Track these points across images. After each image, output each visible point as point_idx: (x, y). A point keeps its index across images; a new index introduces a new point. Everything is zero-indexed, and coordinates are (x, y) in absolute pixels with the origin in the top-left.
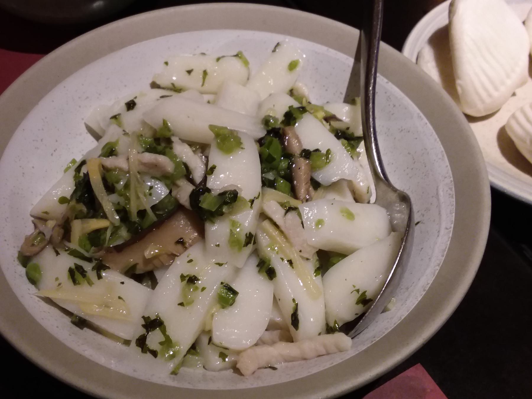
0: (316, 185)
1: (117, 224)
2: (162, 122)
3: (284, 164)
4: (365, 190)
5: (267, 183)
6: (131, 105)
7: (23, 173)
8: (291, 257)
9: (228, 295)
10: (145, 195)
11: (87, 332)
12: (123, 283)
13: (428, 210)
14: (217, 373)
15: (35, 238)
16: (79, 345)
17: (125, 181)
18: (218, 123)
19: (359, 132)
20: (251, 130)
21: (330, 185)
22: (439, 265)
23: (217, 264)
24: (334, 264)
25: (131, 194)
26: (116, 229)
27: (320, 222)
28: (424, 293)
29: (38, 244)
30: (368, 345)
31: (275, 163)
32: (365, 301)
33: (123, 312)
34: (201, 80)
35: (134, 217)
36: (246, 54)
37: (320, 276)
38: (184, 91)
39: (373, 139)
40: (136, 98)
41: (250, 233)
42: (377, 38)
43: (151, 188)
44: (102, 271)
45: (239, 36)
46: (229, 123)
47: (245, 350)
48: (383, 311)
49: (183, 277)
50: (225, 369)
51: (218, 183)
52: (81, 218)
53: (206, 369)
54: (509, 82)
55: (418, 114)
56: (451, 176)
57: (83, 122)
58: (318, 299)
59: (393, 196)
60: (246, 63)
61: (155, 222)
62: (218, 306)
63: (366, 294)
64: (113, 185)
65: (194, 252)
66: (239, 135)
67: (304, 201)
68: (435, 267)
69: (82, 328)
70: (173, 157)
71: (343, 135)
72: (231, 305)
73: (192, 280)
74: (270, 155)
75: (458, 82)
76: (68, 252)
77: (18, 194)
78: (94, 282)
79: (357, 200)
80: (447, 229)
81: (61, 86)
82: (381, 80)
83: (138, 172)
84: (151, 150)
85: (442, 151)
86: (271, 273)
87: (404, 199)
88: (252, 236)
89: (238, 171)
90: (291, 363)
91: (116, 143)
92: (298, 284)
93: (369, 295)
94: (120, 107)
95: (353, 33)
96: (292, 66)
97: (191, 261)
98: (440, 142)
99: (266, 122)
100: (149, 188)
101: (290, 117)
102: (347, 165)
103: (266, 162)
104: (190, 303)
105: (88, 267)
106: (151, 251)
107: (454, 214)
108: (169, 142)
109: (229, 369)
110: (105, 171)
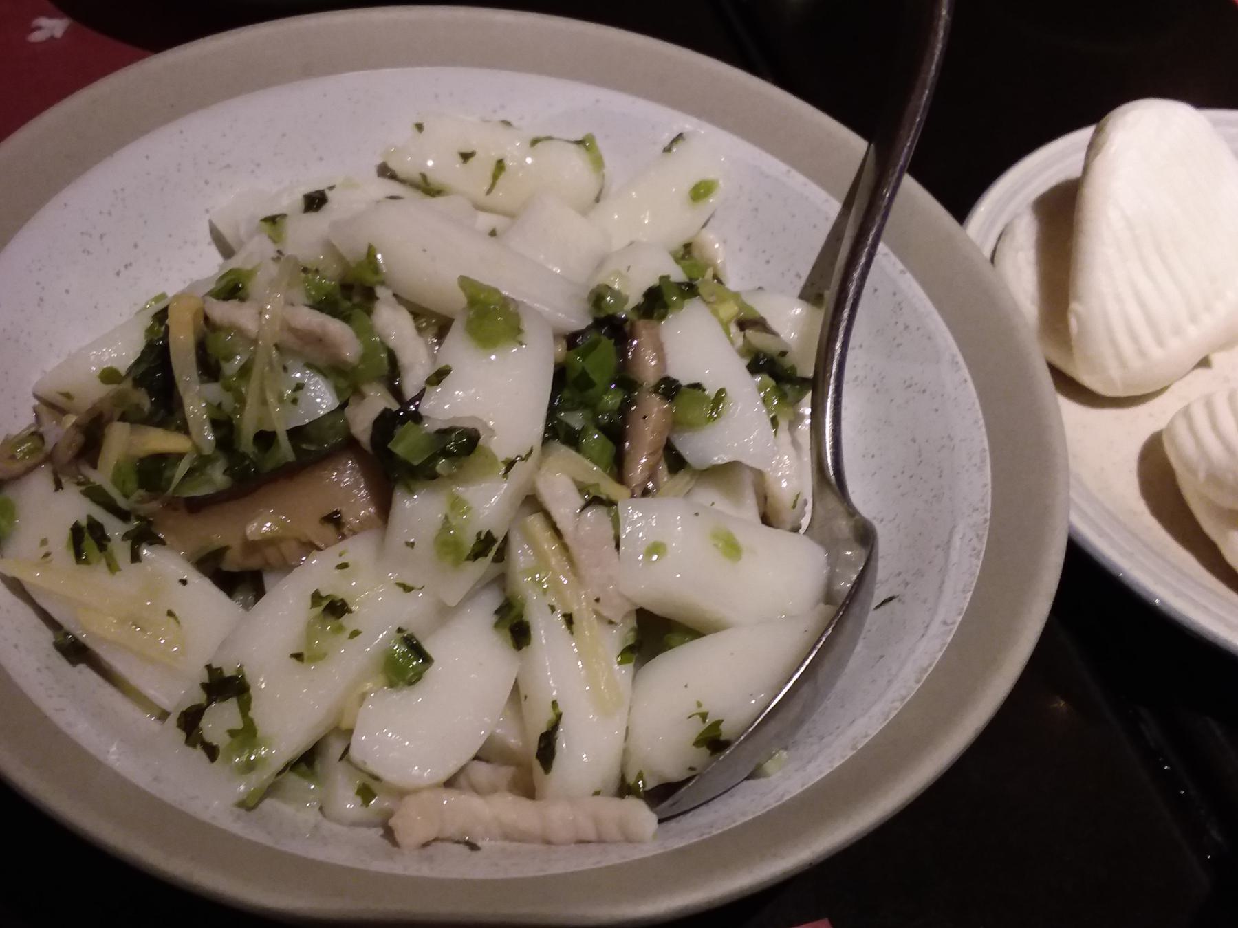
0: (676, 462)
1: (208, 450)
2: (364, 250)
3: (612, 400)
4: (788, 500)
5: (557, 432)
6: (315, 202)
7: (42, 300)
8: (574, 609)
9: (409, 661)
10: (280, 400)
11: (84, 674)
12: (184, 582)
13: (919, 574)
14: (345, 829)
15: (20, 441)
16: (50, 696)
17: (246, 357)
18: (485, 276)
19: (807, 370)
20: (556, 306)
21: (707, 470)
22: (903, 699)
23: (400, 585)
24: (671, 648)
25: (251, 391)
26: (202, 463)
27: (656, 548)
28: (851, 754)
29: (23, 457)
30: (694, 839)
31: (591, 392)
32: (713, 741)
33: (387, 733)
34: (490, 181)
35: (246, 444)
36: (601, 143)
37: (630, 666)
38: (447, 194)
39: (832, 387)
40: (331, 188)
41: (489, 534)
42: (898, 168)
43: (299, 387)
44: (144, 545)
45: (597, 101)
46: (506, 279)
47: (416, 791)
48: (750, 777)
49: (316, 598)
50: (369, 825)
51: (445, 407)
52: (133, 422)
53: (325, 816)
54: (1193, 332)
55: (954, 356)
56: (989, 508)
57: (207, 217)
58: (612, 716)
59: (843, 526)
60: (598, 163)
61: (288, 464)
62: (381, 679)
63: (723, 727)
64: (217, 362)
65: (358, 549)
66: (1072, 481)
67: (638, 492)
68: (893, 702)
69: (74, 663)
70: (365, 332)
71: (767, 365)
72: (411, 683)
73: (336, 609)
74: (584, 374)
75: (1074, 306)
76: (83, 488)
77: (17, 341)
78: (121, 566)
79: (766, 520)
80: (945, 623)
81: (172, 129)
82: (886, 260)
83: (276, 346)
84: (326, 305)
85: (984, 450)
86: (520, 634)
87: (865, 536)
88: (494, 541)
89: (499, 392)
90: (515, 845)
91: (250, 274)
92: (576, 672)
93: (726, 731)
94: (290, 202)
95: (855, 146)
96: (700, 192)
97: (344, 566)
98: (984, 429)
99: (597, 298)
100: (294, 386)
101: (656, 302)
102: (746, 428)
103: (567, 384)
104: (318, 657)
105: (115, 529)
106: (264, 527)
107: (969, 595)
108: (369, 296)
109: (375, 826)
110: (208, 327)
